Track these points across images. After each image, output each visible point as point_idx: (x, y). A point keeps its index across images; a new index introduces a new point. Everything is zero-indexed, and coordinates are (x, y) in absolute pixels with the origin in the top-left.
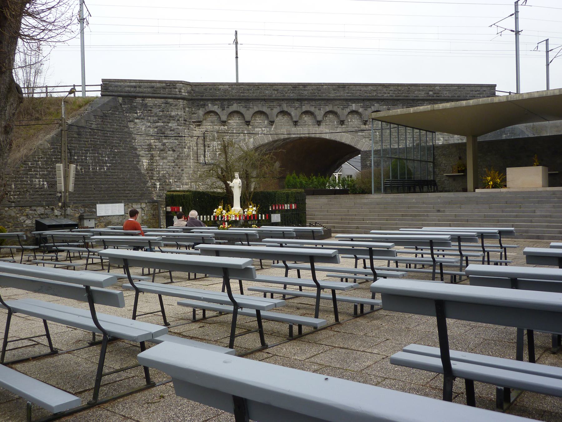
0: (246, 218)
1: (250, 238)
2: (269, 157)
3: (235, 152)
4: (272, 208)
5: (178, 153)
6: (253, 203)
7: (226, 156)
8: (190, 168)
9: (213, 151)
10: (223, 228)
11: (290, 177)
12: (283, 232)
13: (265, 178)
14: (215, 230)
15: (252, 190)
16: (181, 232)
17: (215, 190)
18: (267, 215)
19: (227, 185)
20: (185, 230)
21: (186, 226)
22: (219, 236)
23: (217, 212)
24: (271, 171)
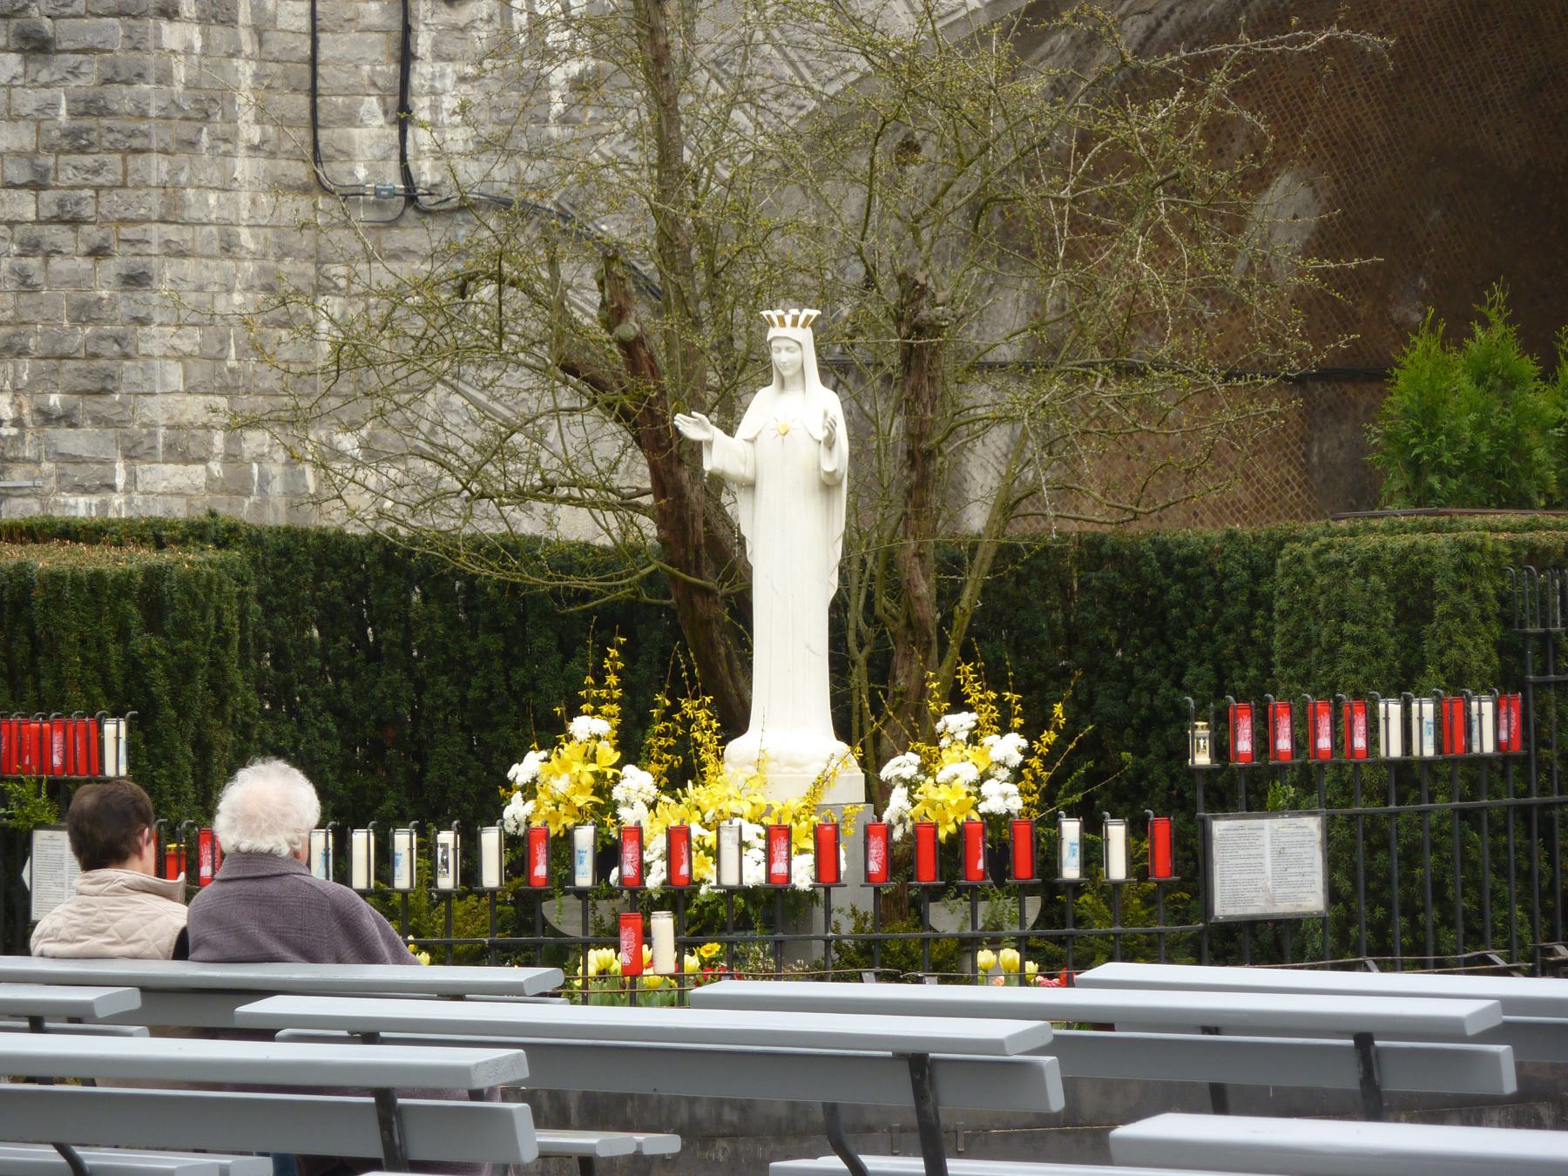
0: (900, 862)
1: (953, 1104)
2: (1181, 124)
3: (772, 64)
4: (1221, 749)
5: (91, 70)
6: (993, 678)
7: (665, 107)
8: (229, 248)
9: (502, 47)
10: (628, 989)
11: (1443, 374)
12: (1363, 1039)
13: (1128, 371)
14: (522, 1003)
15: (976, 519)
16: (117, 1023)
17: (528, 523)
18: (1162, 828)
19: (672, 461)
20: (164, 1006)
21: (182, 950)
22: (576, 1082)
23: (557, 777)
24: (1210, 292)
